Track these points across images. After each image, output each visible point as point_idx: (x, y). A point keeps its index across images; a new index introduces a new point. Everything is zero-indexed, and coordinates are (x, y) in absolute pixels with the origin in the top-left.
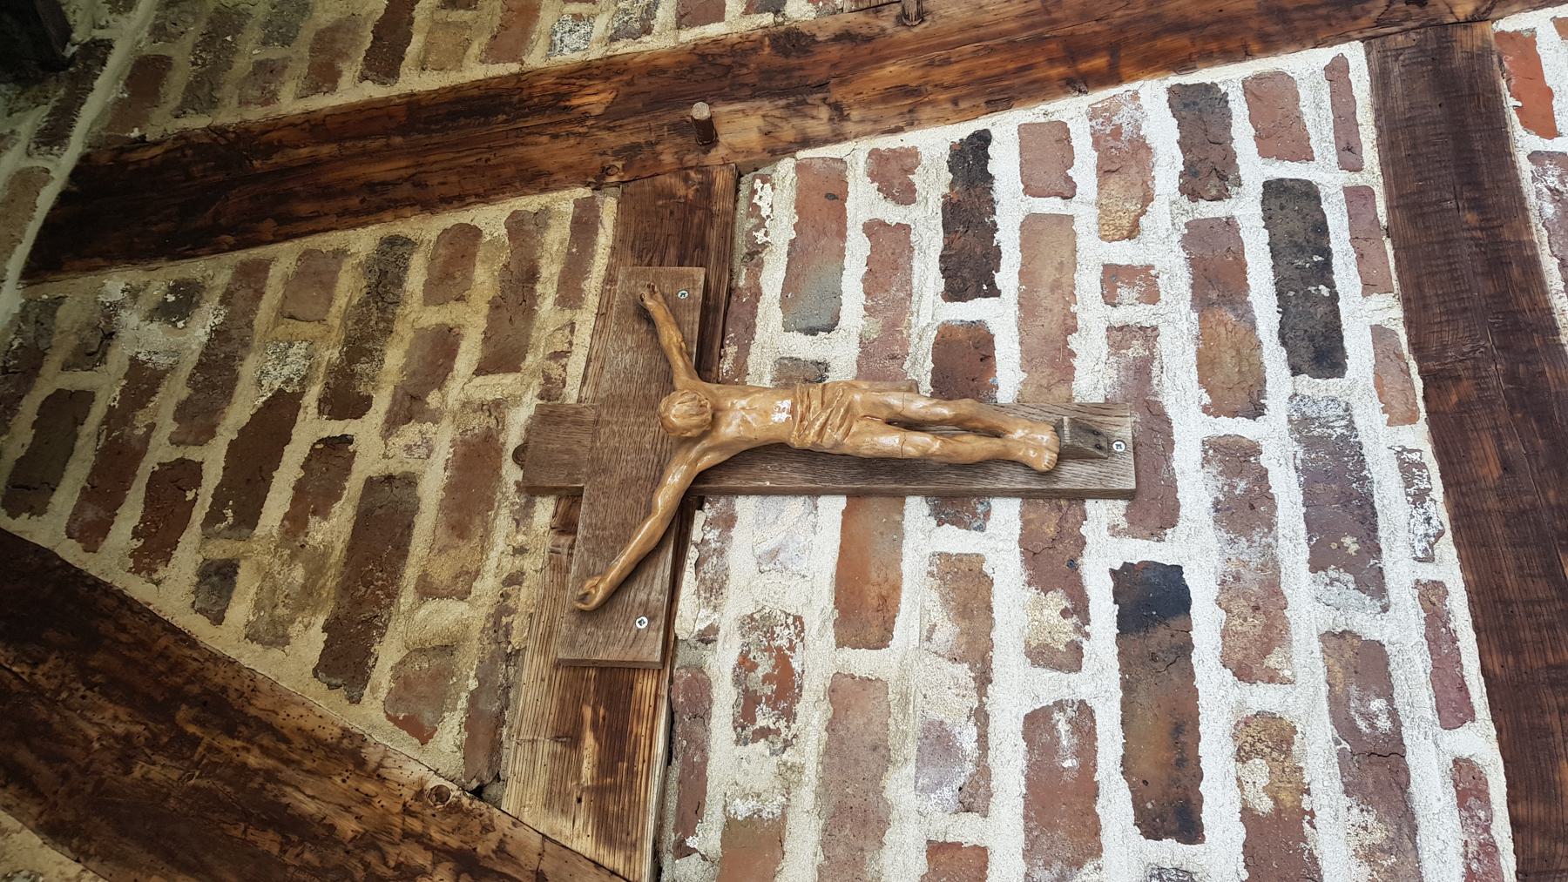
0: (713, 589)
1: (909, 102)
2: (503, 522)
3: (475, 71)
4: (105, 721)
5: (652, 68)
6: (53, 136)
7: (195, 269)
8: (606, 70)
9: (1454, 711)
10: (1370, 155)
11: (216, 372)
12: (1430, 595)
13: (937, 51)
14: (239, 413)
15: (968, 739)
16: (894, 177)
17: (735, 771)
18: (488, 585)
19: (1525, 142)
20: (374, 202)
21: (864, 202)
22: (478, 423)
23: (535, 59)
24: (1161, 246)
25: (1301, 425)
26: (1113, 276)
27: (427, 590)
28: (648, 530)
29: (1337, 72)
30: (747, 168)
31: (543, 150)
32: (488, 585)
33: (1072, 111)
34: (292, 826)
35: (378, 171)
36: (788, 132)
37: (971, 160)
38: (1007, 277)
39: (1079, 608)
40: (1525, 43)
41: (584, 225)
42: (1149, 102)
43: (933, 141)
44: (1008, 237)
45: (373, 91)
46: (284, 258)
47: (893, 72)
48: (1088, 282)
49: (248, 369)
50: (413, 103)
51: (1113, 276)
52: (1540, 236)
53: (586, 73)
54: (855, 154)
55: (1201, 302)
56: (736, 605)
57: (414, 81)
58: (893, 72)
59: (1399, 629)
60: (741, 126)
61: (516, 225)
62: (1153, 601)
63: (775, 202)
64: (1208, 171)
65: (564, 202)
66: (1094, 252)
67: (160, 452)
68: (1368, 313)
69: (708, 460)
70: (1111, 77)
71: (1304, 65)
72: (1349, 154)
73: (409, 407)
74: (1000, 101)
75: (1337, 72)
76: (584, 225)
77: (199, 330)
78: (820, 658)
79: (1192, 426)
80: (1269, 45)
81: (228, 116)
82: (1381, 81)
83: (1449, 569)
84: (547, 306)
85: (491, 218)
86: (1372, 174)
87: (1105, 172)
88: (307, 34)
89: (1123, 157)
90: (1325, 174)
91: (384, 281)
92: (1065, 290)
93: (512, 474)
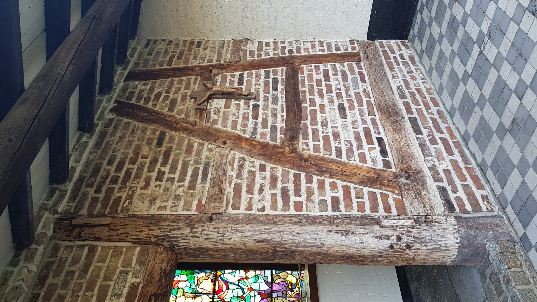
0: (212, 105)
1: (235, 70)
2: (188, 101)
3: (181, 66)
4: (143, 114)
5: (204, 66)
6: (125, 69)
7: (147, 82)
8: (198, 66)
9: (282, 111)
10: (284, 76)
11: (151, 90)
12: (282, 106)
13: (240, 66)
14: (155, 93)
15: (237, 114)
16: (233, 76)
17: (213, 116)
18: (186, 105)
19: (300, 75)
20: (169, 76)
21: (229, 78)
22: (184, 94)
23: (189, 65)
24: (262, 82)
25: (273, 95)
26: (256, 84)
27: (179, 106)
28: (205, 98)
29: (282, 70)
30: (215, 75)
31: (190, 73)
32: (186, 105)
33: (254, 72)
34: (166, 120)
35: (170, 74)
36: (221, 72)
37: (242, 76)
38: (245, 84)
39: (249, 106)
40: (303, 68)
41: (196, 79)
42: (262, 72)
43: (237, 74)
44: (245, 81)
45: (168, 67)
46: (158, 81)
47: (233, 68)
48: (253, 85)
49: (156, 90)
50: (173, 68)
51: (256, 84)
52: (299, 82)
53: (196, 66)
54: (228, 74)
55: (264, 86)
56: (213, 107)
57: (173, 66)
58: (233, 68)
59: (279, 108)
60: (215, 71)
61: (188, 79)
62: (256, 107)
63: (219, 78)
64: (267, 76)
65: (194, 77)
66: (254, 82)
67: (145, 96)
68: (281, 87)
69: (212, 93)
70: (258, 69)
71: (279, 69)
72: (282, 75)
73: (176, 92)
74: (245, 71)
75: (282, 70)
76: (196, 79)
77: (149, 87)
78: (222, 110)
79: (262, 94)
80: (276, 67)
81: (149, 68)
82: (287, 70)
83: (284, 104)
84: (192, 85)
85: (185, 78)
86: (284, 77)
87: (256, 76)
88: (159, 61)
89: (258, 76)
90: (279, 77)
91: (172, 83)
92: (251, 85)
93: (188, 97)
